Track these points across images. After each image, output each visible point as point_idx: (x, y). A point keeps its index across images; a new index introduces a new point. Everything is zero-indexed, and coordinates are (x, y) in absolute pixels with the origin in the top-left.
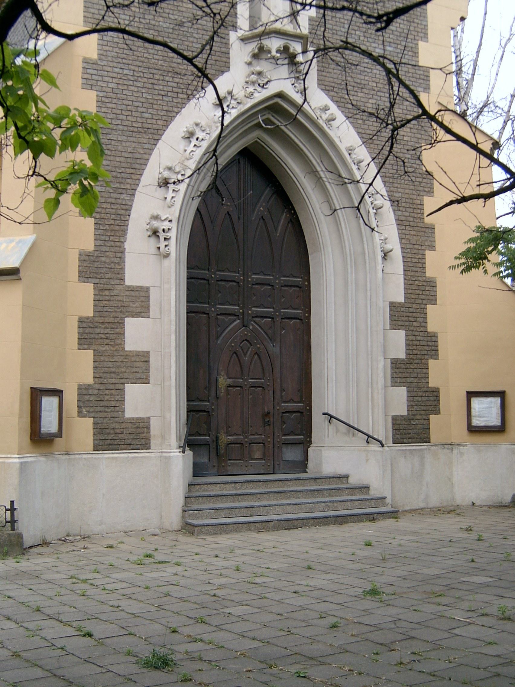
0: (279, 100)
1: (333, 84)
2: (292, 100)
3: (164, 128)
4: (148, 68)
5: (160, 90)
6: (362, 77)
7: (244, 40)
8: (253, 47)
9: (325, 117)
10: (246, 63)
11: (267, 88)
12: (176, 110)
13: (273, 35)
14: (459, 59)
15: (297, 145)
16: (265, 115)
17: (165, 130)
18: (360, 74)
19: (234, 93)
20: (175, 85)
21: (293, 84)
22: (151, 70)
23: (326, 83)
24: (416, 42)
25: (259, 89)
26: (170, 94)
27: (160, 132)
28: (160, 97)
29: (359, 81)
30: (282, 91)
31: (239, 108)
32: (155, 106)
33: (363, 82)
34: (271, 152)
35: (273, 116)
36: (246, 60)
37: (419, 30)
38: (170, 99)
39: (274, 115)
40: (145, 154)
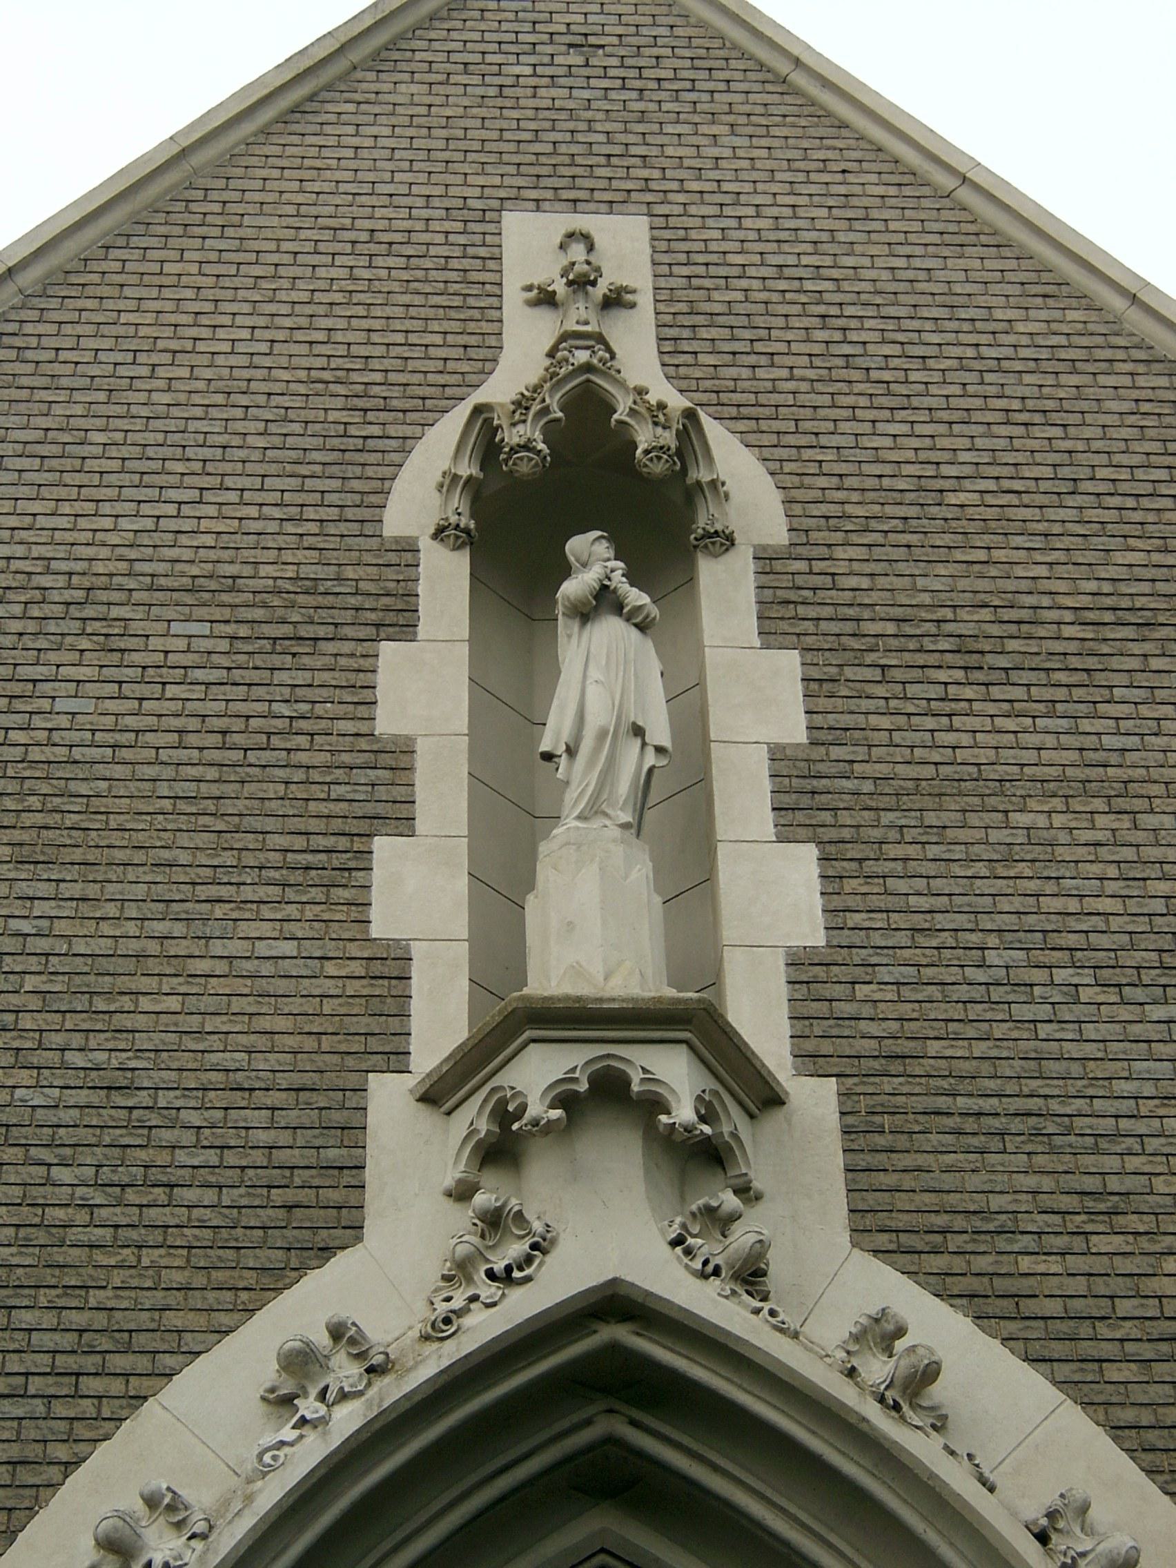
0: (624, 1334)
1: (940, 1221)
2: (674, 1314)
6: (1112, 1163)
9: (877, 1369)
11: (528, 1279)
12: (61, 1452)
13: (528, 1034)
15: (786, 1543)
16: (588, 1422)
18: (1096, 1151)
19: (1092, 1513)
20: (67, 1341)
21: (677, 1242)
23: (901, 1221)
25: (488, 1291)
26: (35, 1385)
29: (1091, 1183)
30: (615, 1281)
31: (371, 1393)
33: (1114, 1184)
35: (634, 1423)
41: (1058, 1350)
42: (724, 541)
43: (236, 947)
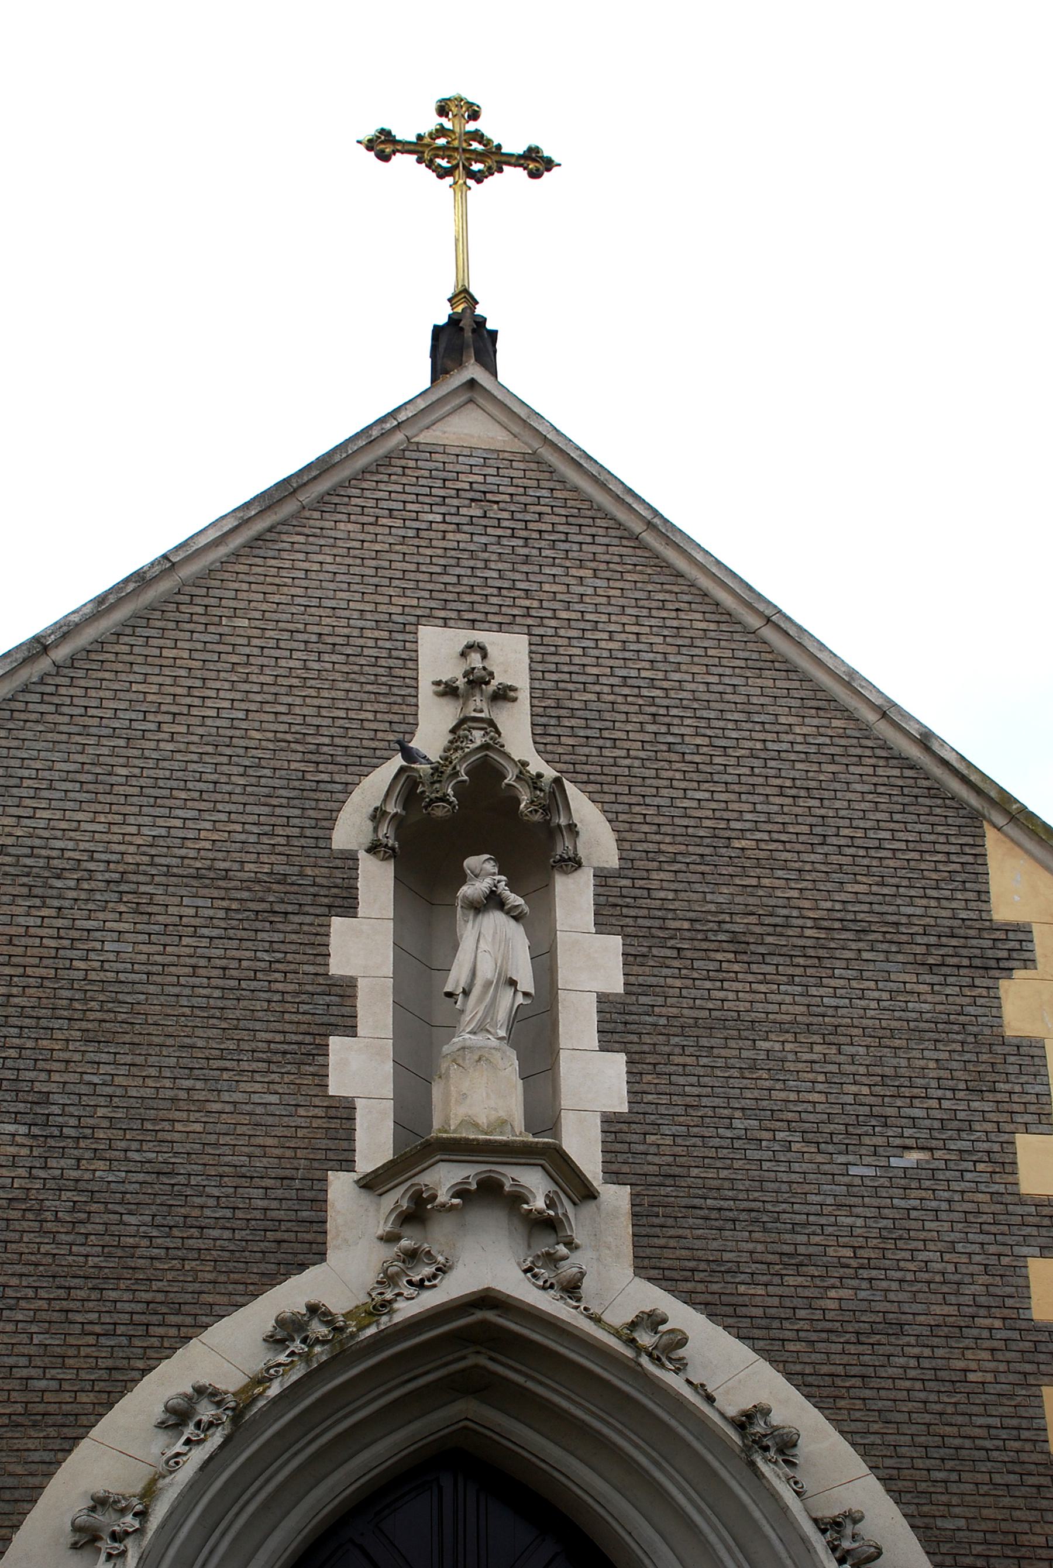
0: (491, 1316)
3: (101, 1410)
4: (54, 1277)
5: (91, 1323)
7: (371, 1184)
8: (397, 1198)
10: (381, 1238)
11: (435, 1286)
12: (140, 1364)
14: (269, 536)
17: (102, 1415)
21: (526, 1271)
22: (59, 1281)
24: (1005, 1137)
25: (408, 1291)
27: (83, 1420)
28: (91, 1340)
30: (488, 1289)
32: (70, 1362)
34: (520, 1450)
35: (491, 1359)
36: (380, 1232)
37: (1016, 1108)
38: (124, 1341)
39: (493, 1354)
40: (31, 1474)
41: (757, 1333)
42: (573, 863)
43: (237, 1097)
